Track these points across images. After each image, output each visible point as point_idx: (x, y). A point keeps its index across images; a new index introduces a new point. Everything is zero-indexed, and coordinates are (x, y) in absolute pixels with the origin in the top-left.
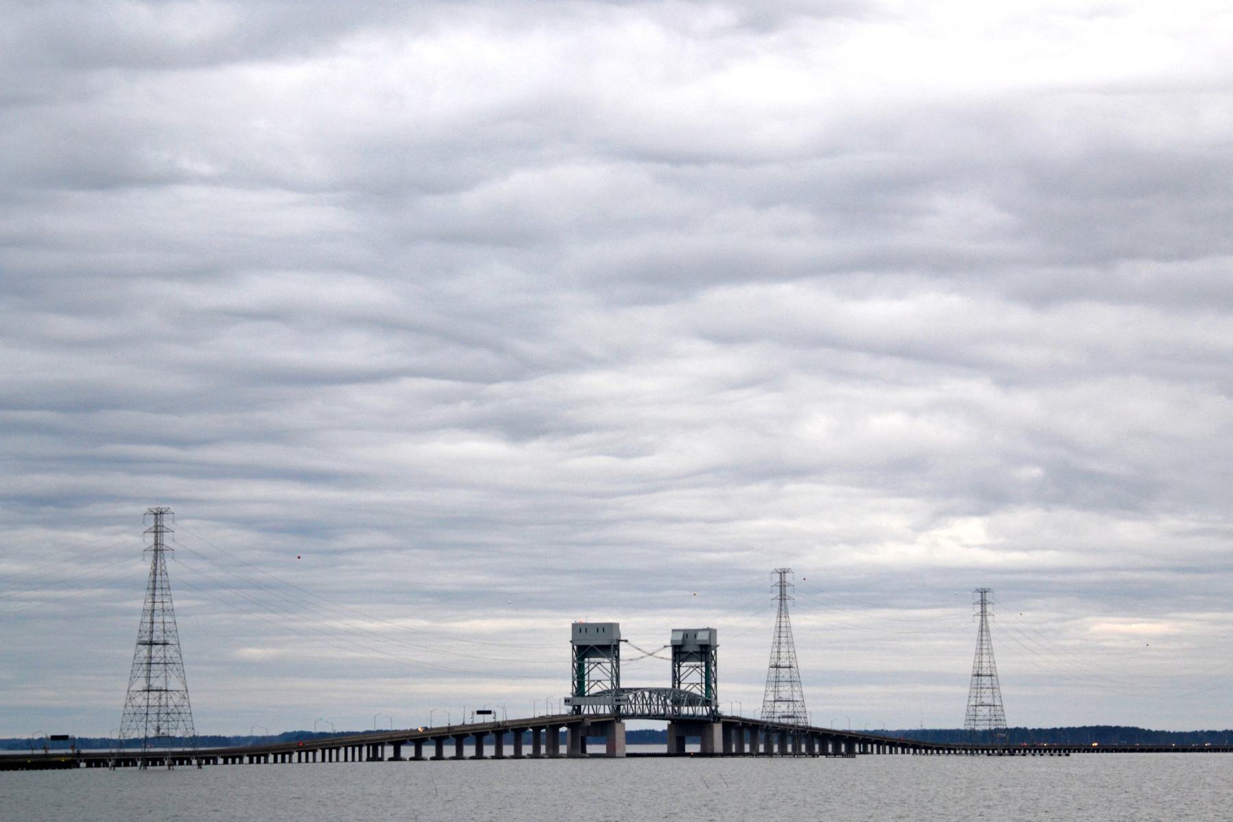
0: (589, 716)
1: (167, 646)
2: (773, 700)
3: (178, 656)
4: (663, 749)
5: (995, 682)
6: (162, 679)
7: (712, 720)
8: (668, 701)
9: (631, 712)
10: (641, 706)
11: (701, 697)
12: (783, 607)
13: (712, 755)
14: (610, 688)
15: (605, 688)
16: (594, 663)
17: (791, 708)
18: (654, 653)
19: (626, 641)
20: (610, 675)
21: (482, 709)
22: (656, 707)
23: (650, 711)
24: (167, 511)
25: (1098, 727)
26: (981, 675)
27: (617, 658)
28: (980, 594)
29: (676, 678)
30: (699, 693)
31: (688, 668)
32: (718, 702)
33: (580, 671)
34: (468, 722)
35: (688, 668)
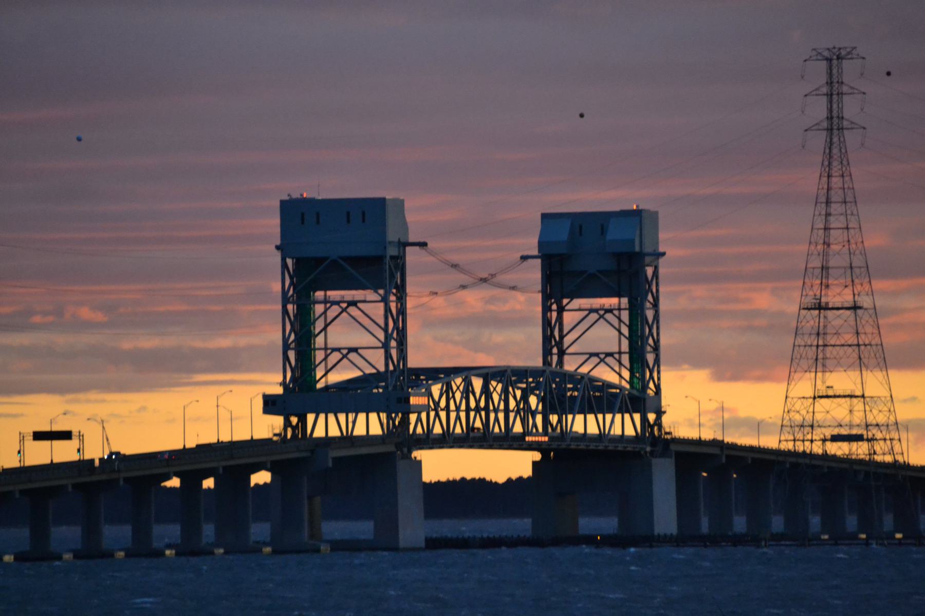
0: (327, 441)
1: (859, 312)
2: (810, 393)
4: (522, 526)
7: (648, 449)
8: (533, 400)
9: (437, 430)
10: (463, 415)
11: (621, 388)
12: (835, 151)
13: (650, 540)
14: (382, 369)
15: (370, 370)
16: (337, 303)
18: (493, 276)
19: (423, 245)
20: (381, 336)
21: (46, 428)
22: (501, 416)
23: (486, 424)
24: (849, 53)
31: (586, 312)
32: (663, 403)
33: (303, 325)
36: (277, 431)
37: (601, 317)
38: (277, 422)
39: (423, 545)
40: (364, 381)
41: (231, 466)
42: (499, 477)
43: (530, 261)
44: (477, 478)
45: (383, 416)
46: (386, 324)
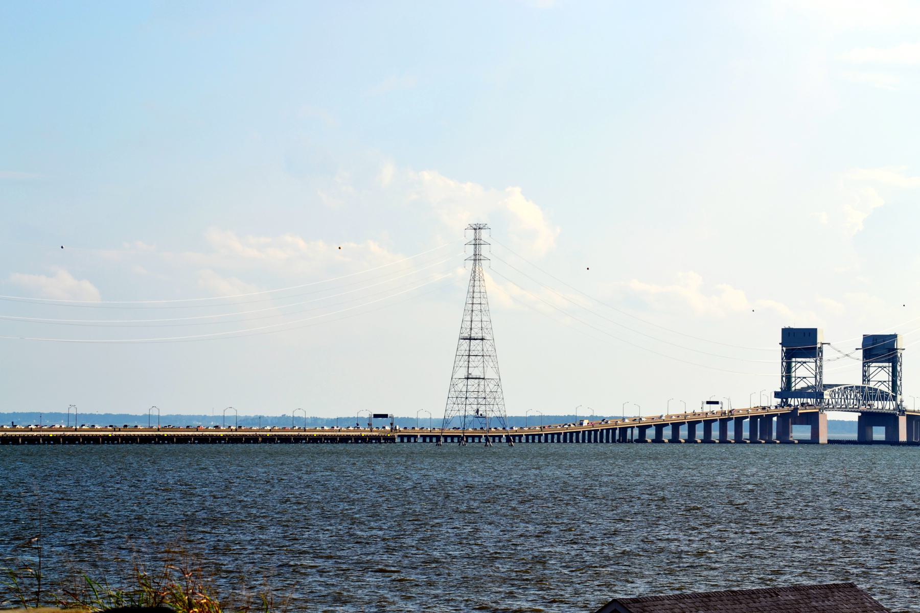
3: (493, 349)
7: (898, 413)
14: (814, 384)
16: (800, 362)
24: (484, 226)
29: (866, 377)
30: (886, 390)
34: (698, 411)
37: (802, 364)
38: (779, 400)
39: (827, 442)
41: (768, 415)
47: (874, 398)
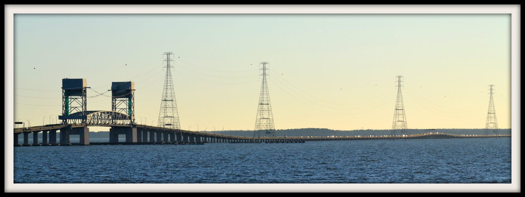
0: (71, 125)
1: (173, 101)
5: (269, 108)
6: (268, 115)
12: (168, 71)
15: (79, 111)
16: (73, 98)
17: (172, 121)
20: (82, 105)
22: (97, 120)
25: (354, 130)
26: (263, 104)
27: (85, 96)
28: (398, 78)
29: (114, 107)
31: (120, 101)
32: (135, 118)
33: (66, 103)
35: (120, 101)
36: (61, 123)
38: (62, 121)
39: (89, 144)
40: (78, 113)
42: (96, 131)
43: (110, 91)
44: (377, 130)
45: (81, 120)
46: (82, 102)
47: (118, 118)
